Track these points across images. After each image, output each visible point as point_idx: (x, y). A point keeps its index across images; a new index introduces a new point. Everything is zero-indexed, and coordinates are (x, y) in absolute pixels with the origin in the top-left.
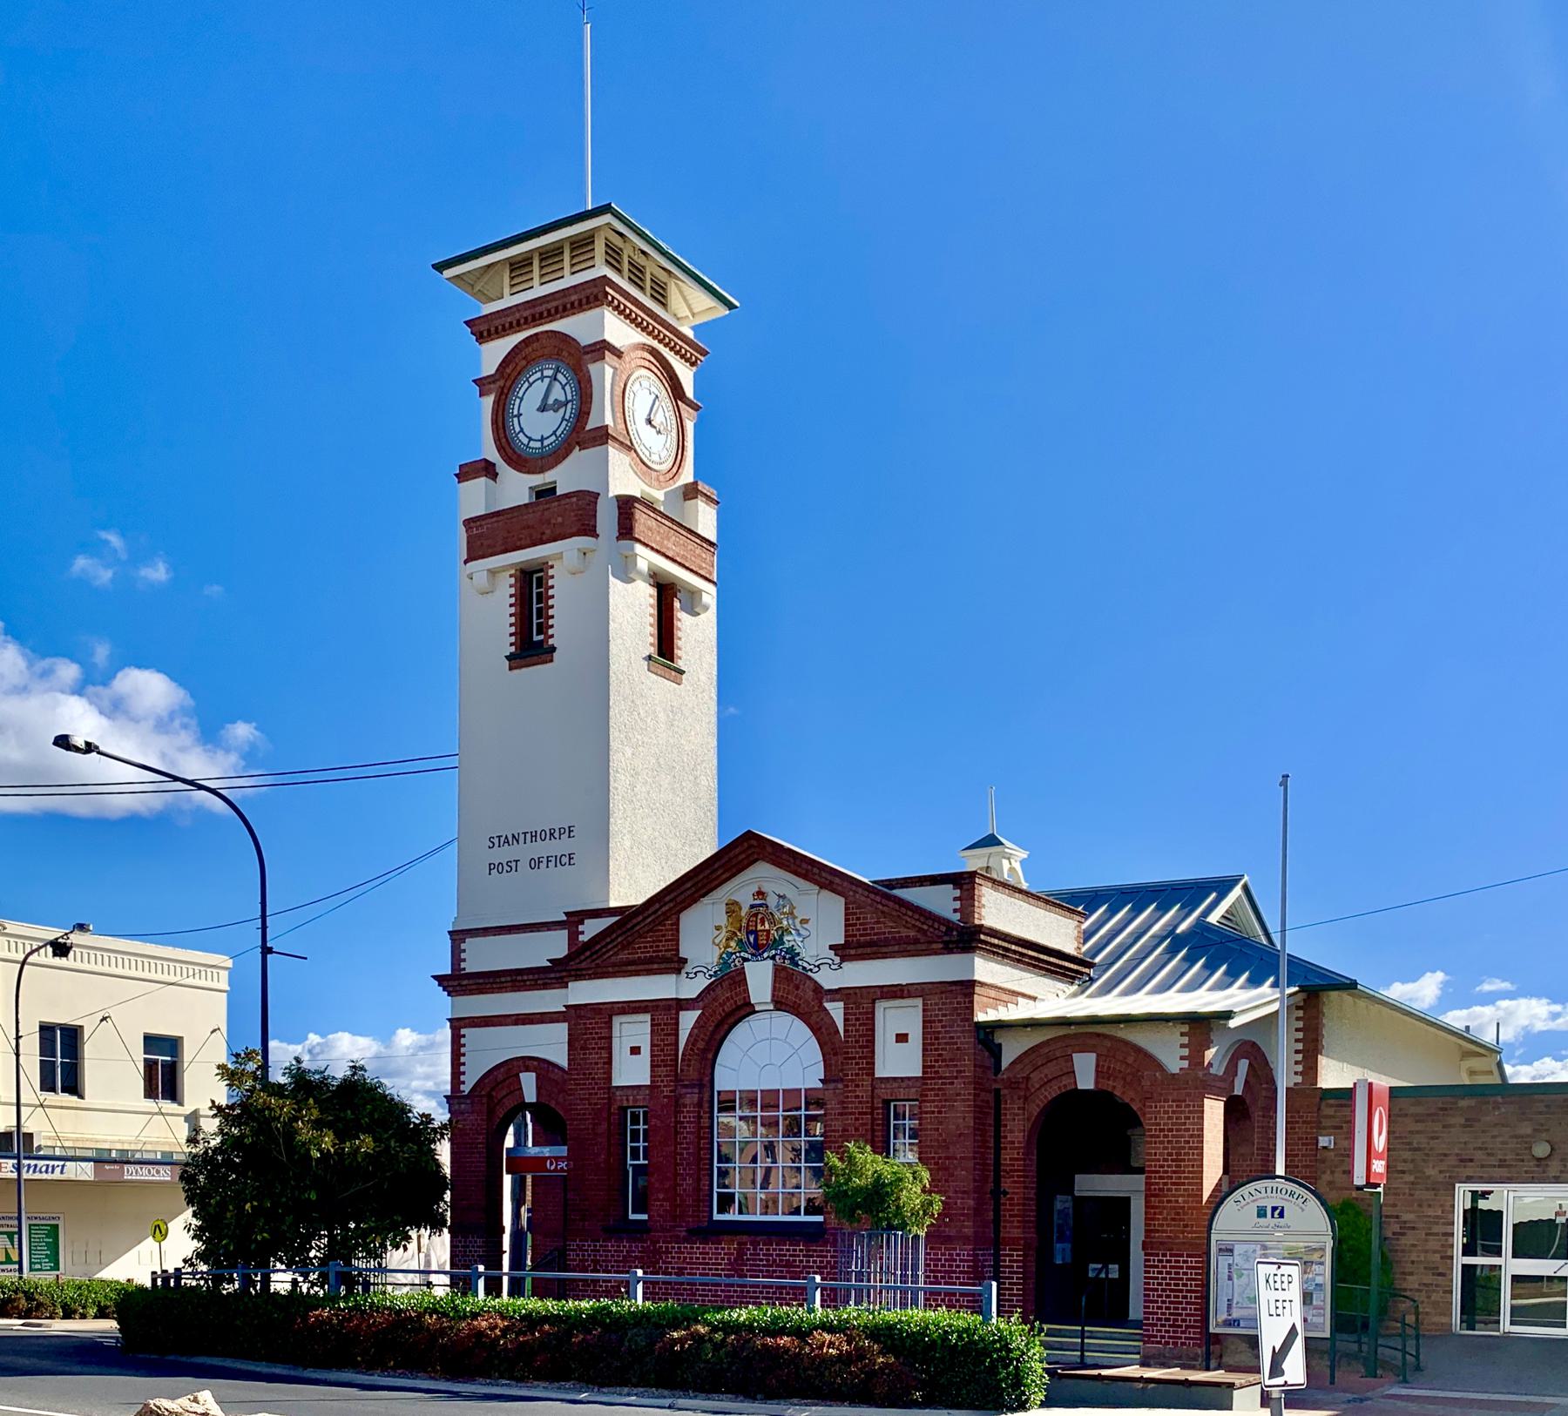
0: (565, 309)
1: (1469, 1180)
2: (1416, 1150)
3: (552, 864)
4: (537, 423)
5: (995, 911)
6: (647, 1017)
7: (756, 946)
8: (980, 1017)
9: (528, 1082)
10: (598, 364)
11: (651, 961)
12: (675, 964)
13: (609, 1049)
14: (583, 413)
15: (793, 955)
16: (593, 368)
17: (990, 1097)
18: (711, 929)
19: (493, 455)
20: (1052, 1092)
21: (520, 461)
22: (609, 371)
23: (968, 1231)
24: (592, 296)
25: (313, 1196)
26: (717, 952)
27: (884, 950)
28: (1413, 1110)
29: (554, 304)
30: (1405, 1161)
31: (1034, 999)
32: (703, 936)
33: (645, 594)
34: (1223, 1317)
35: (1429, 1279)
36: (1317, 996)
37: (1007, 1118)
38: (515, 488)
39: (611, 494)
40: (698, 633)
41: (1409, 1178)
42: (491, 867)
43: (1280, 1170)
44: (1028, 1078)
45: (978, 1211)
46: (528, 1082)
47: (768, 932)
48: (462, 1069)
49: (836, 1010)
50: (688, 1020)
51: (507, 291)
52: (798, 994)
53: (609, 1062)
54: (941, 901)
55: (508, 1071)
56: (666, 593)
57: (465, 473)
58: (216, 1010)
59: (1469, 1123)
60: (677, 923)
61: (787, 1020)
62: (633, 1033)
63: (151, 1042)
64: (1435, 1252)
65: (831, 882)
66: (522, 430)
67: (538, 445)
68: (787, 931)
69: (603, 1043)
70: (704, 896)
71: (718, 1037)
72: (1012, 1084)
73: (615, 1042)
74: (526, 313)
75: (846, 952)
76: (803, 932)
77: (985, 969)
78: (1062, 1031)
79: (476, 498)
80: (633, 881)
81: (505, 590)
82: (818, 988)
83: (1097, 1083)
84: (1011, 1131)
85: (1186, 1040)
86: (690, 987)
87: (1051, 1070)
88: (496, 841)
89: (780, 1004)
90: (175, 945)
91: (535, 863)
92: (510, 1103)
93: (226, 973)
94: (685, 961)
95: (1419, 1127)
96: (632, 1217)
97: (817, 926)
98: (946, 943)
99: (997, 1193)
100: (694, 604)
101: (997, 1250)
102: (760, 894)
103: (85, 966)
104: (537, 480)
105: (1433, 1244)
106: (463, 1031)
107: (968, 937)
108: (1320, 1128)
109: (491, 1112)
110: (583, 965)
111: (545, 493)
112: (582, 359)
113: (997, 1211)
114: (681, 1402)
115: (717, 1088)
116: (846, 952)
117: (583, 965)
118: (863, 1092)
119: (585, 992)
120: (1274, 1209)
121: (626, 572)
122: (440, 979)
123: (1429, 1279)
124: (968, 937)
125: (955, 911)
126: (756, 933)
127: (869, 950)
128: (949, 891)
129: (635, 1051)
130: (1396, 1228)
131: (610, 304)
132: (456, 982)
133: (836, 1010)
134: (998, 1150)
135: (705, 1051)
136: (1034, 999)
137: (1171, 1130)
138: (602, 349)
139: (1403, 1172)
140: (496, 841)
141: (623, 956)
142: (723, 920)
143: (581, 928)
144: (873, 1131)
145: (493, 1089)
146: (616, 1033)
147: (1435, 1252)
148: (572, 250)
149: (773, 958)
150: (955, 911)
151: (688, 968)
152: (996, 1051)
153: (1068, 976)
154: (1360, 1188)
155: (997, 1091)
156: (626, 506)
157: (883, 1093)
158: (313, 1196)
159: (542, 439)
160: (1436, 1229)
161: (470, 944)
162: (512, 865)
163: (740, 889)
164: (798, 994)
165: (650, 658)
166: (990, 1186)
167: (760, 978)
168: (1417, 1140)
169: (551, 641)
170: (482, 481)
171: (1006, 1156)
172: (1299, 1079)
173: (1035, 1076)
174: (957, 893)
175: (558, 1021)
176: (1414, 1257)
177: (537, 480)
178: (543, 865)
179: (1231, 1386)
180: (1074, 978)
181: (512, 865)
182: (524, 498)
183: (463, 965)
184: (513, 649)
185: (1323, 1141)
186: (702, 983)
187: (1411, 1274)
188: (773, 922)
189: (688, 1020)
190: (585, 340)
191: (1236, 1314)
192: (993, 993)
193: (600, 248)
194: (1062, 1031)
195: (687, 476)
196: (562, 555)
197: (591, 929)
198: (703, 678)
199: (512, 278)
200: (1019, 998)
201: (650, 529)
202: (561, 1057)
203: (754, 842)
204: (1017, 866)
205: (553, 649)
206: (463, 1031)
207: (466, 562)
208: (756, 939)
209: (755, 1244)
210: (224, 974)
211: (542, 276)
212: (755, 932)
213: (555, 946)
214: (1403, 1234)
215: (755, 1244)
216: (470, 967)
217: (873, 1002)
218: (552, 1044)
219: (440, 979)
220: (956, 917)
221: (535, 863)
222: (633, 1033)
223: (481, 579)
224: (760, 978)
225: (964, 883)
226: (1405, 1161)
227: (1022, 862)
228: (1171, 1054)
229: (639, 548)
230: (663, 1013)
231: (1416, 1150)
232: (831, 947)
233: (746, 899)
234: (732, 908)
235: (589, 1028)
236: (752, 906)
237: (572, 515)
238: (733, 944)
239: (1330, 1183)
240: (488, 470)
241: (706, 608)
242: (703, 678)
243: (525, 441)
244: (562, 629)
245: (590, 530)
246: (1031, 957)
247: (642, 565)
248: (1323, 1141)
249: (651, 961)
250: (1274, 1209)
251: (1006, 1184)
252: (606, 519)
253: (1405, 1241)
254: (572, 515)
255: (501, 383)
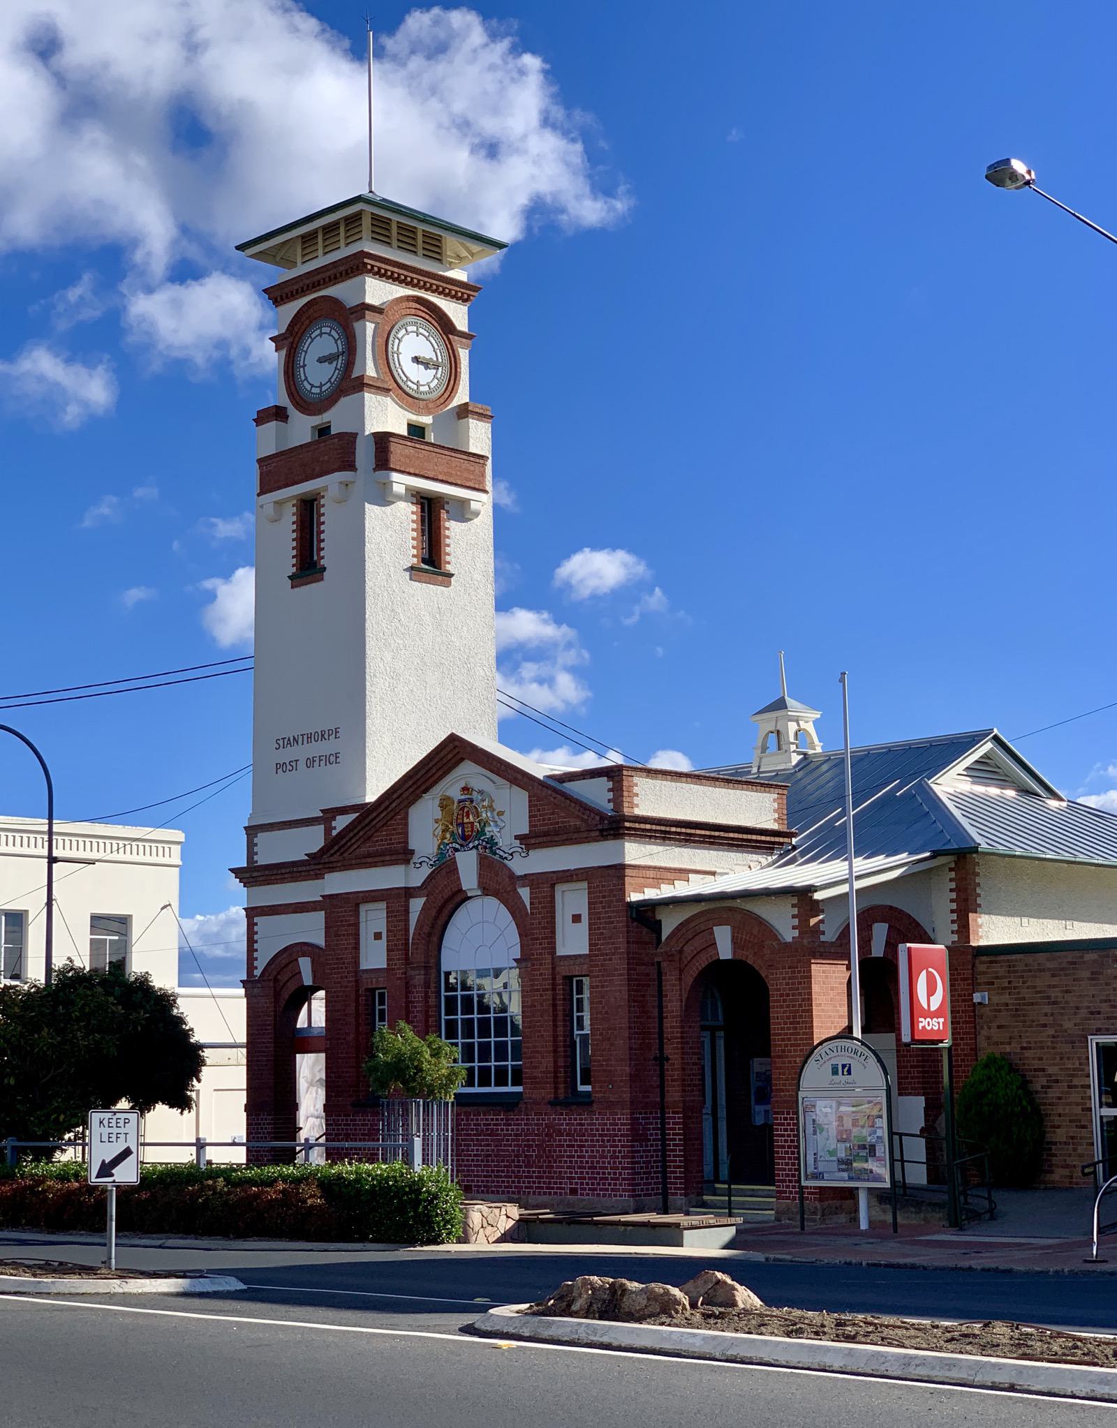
0: (335, 278)
1: (1098, 1031)
2: (1054, 1003)
3: (323, 763)
4: (317, 375)
5: (649, 800)
6: (383, 905)
7: (465, 838)
8: (634, 897)
9: (305, 964)
10: (361, 322)
11: (382, 854)
12: (404, 855)
13: (357, 936)
14: (350, 364)
15: (491, 843)
16: (357, 325)
17: (653, 971)
18: (431, 821)
19: (284, 400)
20: (703, 962)
21: (306, 405)
22: (370, 327)
23: (627, 1096)
24: (356, 266)
25: (12, 1081)
26: (437, 843)
27: (556, 838)
28: (1049, 965)
29: (328, 274)
30: (1046, 1015)
31: (713, 874)
32: (424, 827)
33: (405, 514)
34: (811, 1169)
35: (1073, 1131)
36: (964, 857)
37: (666, 987)
38: (301, 429)
39: (367, 433)
40: (469, 543)
41: (1051, 1032)
42: (280, 767)
43: (857, 1033)
44: (681, 952)
45: (634, 1078)
46: (305, 964)
47: (472, 823)
48: (255, 955)
49: (525, 893)
50: (417, 905)
51: (299, 260)
52: (497, 881)
53: (357, 947)
54: (597, 794)
55: (291, 954)
56: (431, 511)
57: (263, 417)
58: (168, 884)
59: (1094, 976)
60: (406, 818)
61: (492, 903)
62: (374, 920)
63: (98, 922)
64: (1077, 1104)
65: (516, 779)
66: (306, 379)
67: (318, 390)
68: (486, 823)
69: (351, 930)
70: (425, 791)
71: (440, 922)
72: (669, 957)
73: (362, 926)
74: (307, 282)
75: (529, 841)
76: (499, 823)
77: (635, 853)
78: (703, 907)
79: (268, 440)
80: (379, 777)
81: (290, 517)
82: (512, 875)
83: (734, 953)
84: (671, 1001)
85: (795, 911)
86: (416, 876)
87: (698, 943)
88: (281, 742)
89: (486, 890)
90: (124, 824)
91: (310, 762)
92: (292, 987)
93: (179, 847)
94: (412, 852)
95: (1055, 981)
96: (581, 1088)
97: (510, 816)
98: (601, 831)
99: (661, 1059)
100: (463, 511)
101: (663, 1113)
102: (465, 789)
103: (25, 851)
104: (317, 420)
105: (1075, 1097)
106: (256, 920)
107: (616, 826)
108: (975, 986)
109: (277, 995)
110: (332, 859)
111: (323, 431)
112: (347, 317)
113: (662, 1076)
114: (170, 1242)
115: (444, 968)
116: (529, 841)
117: (332, 859)
118: (546, 970)
119: (339, 883)
120: (844, 1066)
121: (384, 497)
122: (237, 872)
123: (1073, 1131)
124: (616, 826)
125: (609, 801)
126: (464, 827)
127: (544, 839)
128: (604, 783)
129: (577, 918)
130: (1043, 1081)
131: (370, 271)
132: (251, 875)
133: (525, 893)
134: (661, 1018)
135: (429, 935)
136: (713, 874)
137: (788, 995)
138: (363, 309)
139: (1045, 1026)
140: (281, 742)
141: (364, 850)
142: (438, 814)
143: (334, 823)
144: (554, 1005)
145: (279, 973)
146: (362, 918)
147: (1077, 1104)
148: (347, 225)
149: (476, 847)
150: (609, 801)
151: (415, 859)
152: (656, 927)
153: (768, 848)
154: (908, 1045)
155: (659, 963)
156: (383, 440)
157: (563, 970)
158: (12, 1081)
159: (321, 386)
160: (1076, 1082)
161: (261, 838)
162: (292, 765)
163: (451, 787)
164: (497, 881)
165: (412, 568)
166: (655, 1052)
167: (468, 865)
168: (1055, 994)
169: (322, 562)
170: (273, 425)
171: (667, 1024)
172: (955, 937)
173: (689, 949)
174: (610, 785)
175: (315, 910)
176: (1060, 1110)
177: (317, 420)
178: (316, 764)
179: (677, 1225)
180: (773, 849)
181: (292, 765)
182: (307, 438)
183: (610, 785)
184: (294, 569)
185: (977, 998)
186: (426, 871)
187: (1059, 1127)
188: (478, 814)
189: (417, 905)
190: (351, 302)
191: (820, 1169)
192: (651, 874)
193: (366, 222)
194: (703, 907)
195: (462, 396)
196: (329, 484)
197: (341, 822)
198: (477, 577)
199: (303, 249)
200: (667, 875)
201: (408, 457)
202: (320, 940)
203: (457, 743)
204: (810, 728)
205: (324, 569)
206: (256, 920)
207: (259, 495)
208: (463, 831)
209: (467, 1114)
210: (176, 849)
211: (303, 256)
212: (462, 824)
213: (314, 840)
214: (1049, 1087)
215: (467, 1114)
216: (262, 860)
217: (553, 886)
218: (312, 928)
219: (237, 872)
220: (611, 806)
221: (310, 762)
222: (374, 920)
223: (270, 510)
224: (468, 865)
225: (613, 774)
226: (1046, 1015)
227: (816, 722)
228: (784, 924)
229: (395, 476)
230: (397, 899)
231: (1054, 1003)
232: (516, 837)
233: (455, 793)
234: (445, 803)
235: (342, 913)
236: (460, 801)
237: (335, 451)
238: (448, 836)
239: (988, 1038)
240: (279, 414)
241: (477, 514)
242: (477, 577)
243: (308, 387)
244: (329, 555)
245: (350, 465)
246: (701, 836)
247: (399, 489)
248: (977, 998)
249: (382, 854)
250: (844, 1066)
251: (669, 1050)
252: (364, 455)
253: (1053, 1093)
254: (335, 451)
255: (291, 340)
